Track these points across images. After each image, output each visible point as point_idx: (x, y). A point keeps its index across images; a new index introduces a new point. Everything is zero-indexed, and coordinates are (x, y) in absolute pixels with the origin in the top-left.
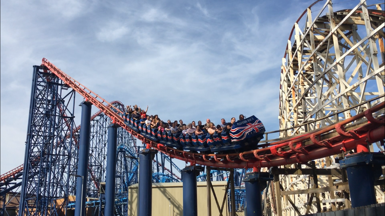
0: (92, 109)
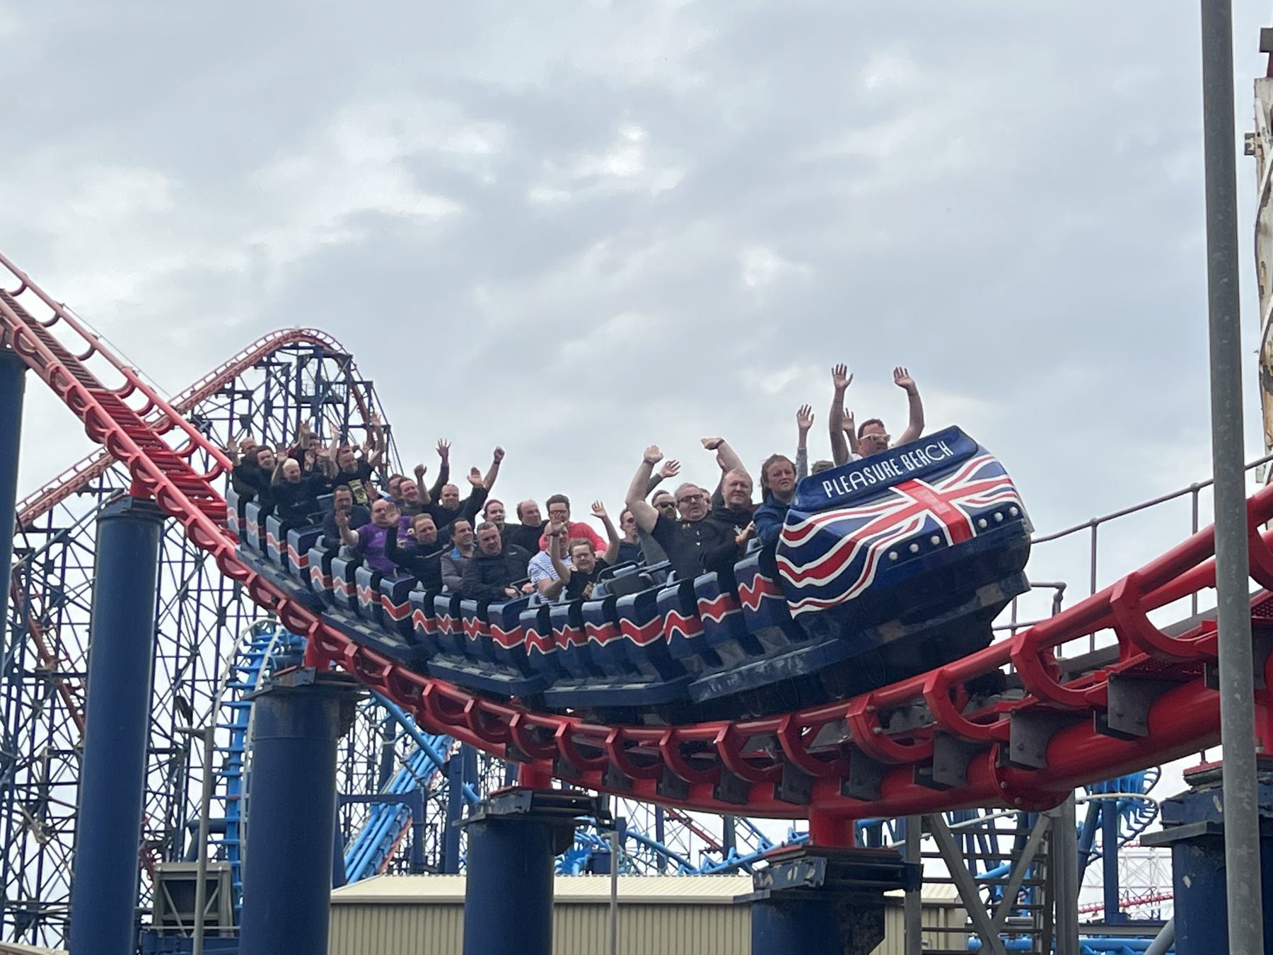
0: (1266, 66)
